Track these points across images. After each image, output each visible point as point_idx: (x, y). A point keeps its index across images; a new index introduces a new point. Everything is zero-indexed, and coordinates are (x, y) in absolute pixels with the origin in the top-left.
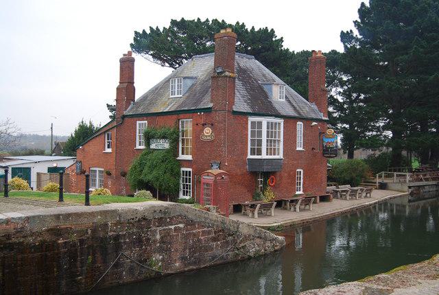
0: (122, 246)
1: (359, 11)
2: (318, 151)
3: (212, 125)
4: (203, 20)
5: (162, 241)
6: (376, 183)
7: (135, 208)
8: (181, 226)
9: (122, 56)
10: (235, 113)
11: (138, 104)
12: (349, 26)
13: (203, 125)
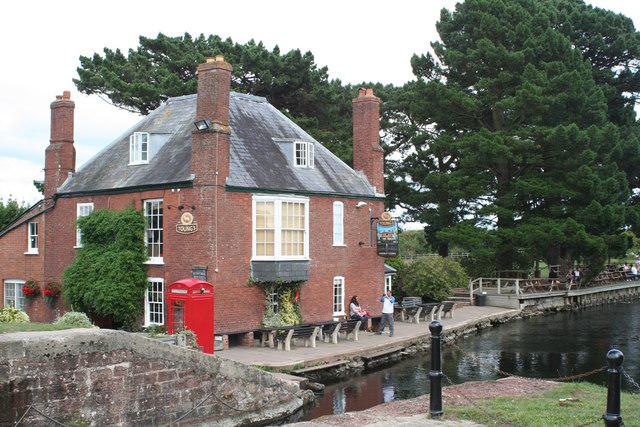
0: (31, 396)
1: (438, 26)
2: (370, 246)
3: (193, 208)
4: (195, 37)
5: (96, 389)
6: (469, 295)
7: (52, 338)
8: (126, 365)
9: (55, 99)
10: (230, 189)
11: (79, 176)
12: (424, 49)
13: (181, 208)
